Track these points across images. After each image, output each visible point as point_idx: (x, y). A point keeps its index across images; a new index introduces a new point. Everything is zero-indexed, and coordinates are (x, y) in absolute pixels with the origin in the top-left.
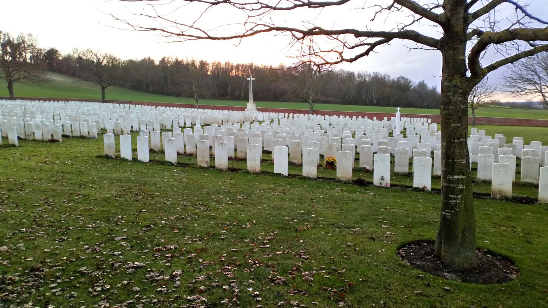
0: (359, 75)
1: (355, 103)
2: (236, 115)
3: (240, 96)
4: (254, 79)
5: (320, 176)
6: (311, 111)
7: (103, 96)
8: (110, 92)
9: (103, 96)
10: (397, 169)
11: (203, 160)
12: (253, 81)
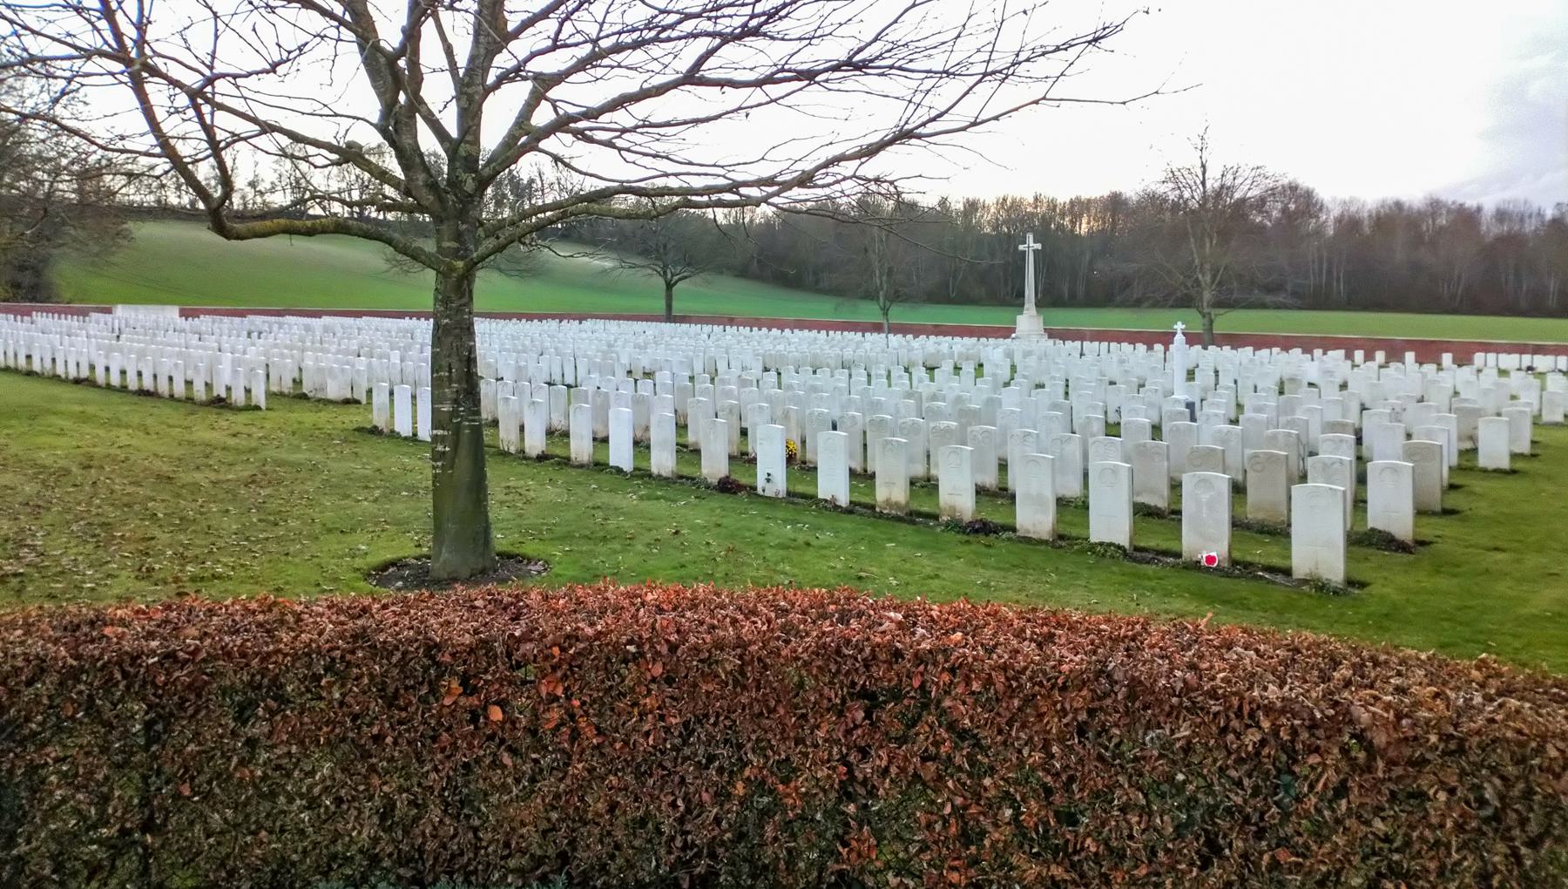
0: (1501, 215)
1: (1474, 306)
2: (993, 351)
3: (1073, 295)
4: (1039, 246)
5: (915, 506)
6: (1206, 338)
7: (669, 307)
8: (688, 293)
9: (669, 307)
10: (1377, 518)
11: (238, 397)
12: (1035, 251)
